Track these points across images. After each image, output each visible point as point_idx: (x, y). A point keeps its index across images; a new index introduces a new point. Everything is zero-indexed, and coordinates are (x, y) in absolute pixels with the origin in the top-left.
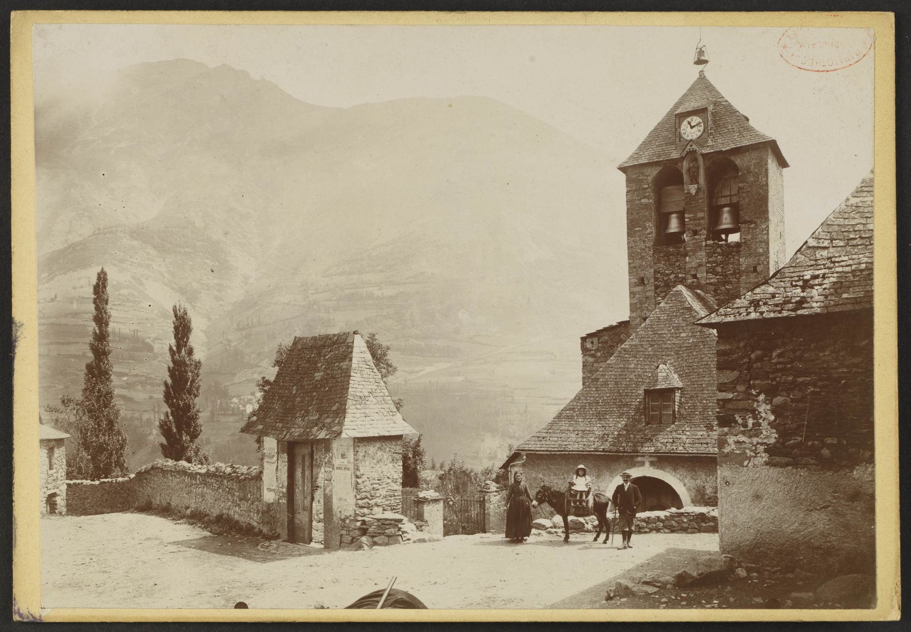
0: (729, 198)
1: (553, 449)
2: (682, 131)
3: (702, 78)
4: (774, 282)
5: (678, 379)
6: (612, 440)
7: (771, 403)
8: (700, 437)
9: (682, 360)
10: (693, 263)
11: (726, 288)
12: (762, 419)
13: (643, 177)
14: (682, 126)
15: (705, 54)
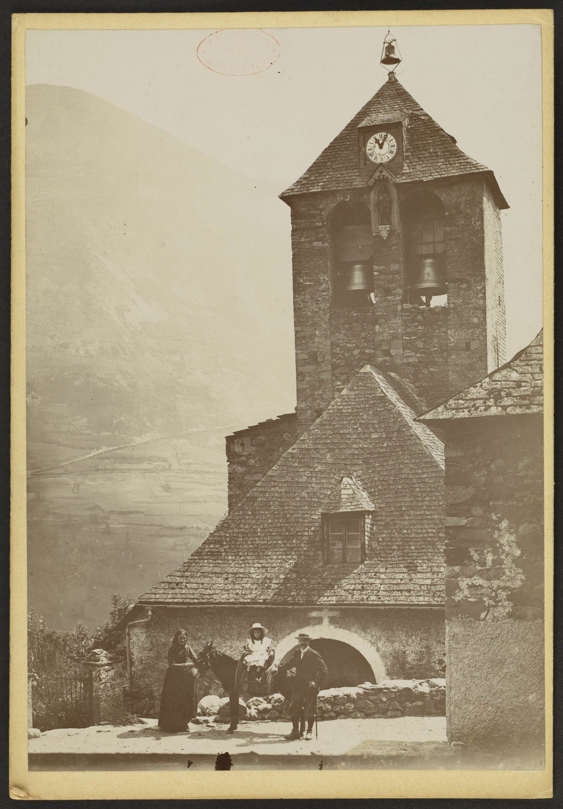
0: (432, 245)
1: (192, 601)
2: (368, 152)
3: (392, 82)
4: (518, 366)
5: (368, 499)
6: (277, 586)
7: (516, 532)
8: (399, 581)
9: (373, 472)
10: (385, 334)
11: (430, 371)
12: (505, 555)
13: (315, 212)
14: (368, 144)
15: (396, 50)
